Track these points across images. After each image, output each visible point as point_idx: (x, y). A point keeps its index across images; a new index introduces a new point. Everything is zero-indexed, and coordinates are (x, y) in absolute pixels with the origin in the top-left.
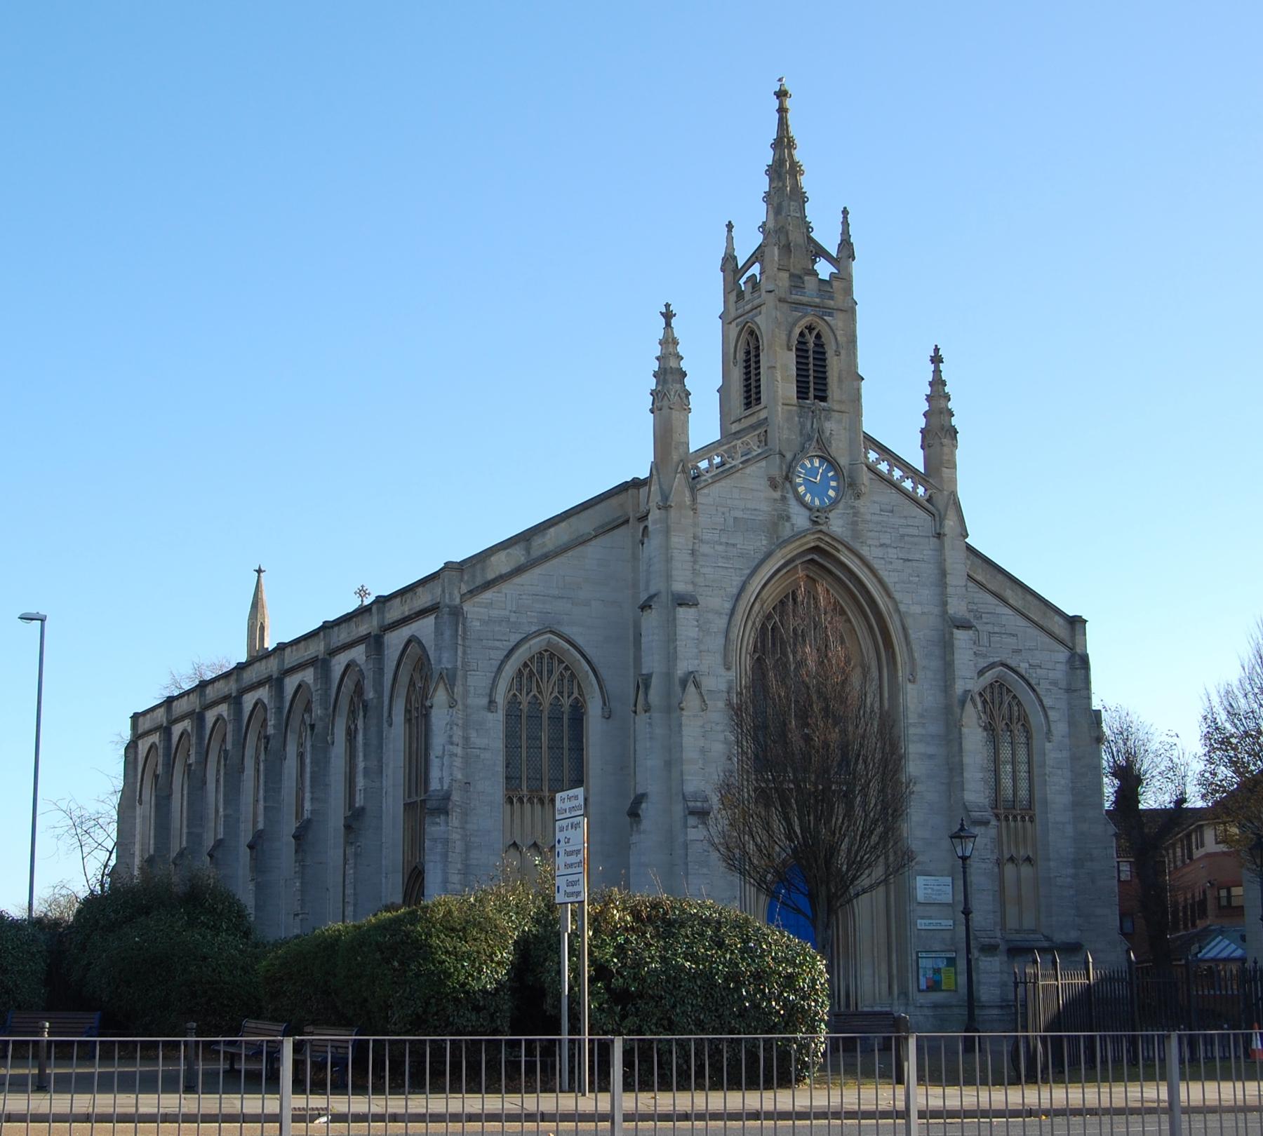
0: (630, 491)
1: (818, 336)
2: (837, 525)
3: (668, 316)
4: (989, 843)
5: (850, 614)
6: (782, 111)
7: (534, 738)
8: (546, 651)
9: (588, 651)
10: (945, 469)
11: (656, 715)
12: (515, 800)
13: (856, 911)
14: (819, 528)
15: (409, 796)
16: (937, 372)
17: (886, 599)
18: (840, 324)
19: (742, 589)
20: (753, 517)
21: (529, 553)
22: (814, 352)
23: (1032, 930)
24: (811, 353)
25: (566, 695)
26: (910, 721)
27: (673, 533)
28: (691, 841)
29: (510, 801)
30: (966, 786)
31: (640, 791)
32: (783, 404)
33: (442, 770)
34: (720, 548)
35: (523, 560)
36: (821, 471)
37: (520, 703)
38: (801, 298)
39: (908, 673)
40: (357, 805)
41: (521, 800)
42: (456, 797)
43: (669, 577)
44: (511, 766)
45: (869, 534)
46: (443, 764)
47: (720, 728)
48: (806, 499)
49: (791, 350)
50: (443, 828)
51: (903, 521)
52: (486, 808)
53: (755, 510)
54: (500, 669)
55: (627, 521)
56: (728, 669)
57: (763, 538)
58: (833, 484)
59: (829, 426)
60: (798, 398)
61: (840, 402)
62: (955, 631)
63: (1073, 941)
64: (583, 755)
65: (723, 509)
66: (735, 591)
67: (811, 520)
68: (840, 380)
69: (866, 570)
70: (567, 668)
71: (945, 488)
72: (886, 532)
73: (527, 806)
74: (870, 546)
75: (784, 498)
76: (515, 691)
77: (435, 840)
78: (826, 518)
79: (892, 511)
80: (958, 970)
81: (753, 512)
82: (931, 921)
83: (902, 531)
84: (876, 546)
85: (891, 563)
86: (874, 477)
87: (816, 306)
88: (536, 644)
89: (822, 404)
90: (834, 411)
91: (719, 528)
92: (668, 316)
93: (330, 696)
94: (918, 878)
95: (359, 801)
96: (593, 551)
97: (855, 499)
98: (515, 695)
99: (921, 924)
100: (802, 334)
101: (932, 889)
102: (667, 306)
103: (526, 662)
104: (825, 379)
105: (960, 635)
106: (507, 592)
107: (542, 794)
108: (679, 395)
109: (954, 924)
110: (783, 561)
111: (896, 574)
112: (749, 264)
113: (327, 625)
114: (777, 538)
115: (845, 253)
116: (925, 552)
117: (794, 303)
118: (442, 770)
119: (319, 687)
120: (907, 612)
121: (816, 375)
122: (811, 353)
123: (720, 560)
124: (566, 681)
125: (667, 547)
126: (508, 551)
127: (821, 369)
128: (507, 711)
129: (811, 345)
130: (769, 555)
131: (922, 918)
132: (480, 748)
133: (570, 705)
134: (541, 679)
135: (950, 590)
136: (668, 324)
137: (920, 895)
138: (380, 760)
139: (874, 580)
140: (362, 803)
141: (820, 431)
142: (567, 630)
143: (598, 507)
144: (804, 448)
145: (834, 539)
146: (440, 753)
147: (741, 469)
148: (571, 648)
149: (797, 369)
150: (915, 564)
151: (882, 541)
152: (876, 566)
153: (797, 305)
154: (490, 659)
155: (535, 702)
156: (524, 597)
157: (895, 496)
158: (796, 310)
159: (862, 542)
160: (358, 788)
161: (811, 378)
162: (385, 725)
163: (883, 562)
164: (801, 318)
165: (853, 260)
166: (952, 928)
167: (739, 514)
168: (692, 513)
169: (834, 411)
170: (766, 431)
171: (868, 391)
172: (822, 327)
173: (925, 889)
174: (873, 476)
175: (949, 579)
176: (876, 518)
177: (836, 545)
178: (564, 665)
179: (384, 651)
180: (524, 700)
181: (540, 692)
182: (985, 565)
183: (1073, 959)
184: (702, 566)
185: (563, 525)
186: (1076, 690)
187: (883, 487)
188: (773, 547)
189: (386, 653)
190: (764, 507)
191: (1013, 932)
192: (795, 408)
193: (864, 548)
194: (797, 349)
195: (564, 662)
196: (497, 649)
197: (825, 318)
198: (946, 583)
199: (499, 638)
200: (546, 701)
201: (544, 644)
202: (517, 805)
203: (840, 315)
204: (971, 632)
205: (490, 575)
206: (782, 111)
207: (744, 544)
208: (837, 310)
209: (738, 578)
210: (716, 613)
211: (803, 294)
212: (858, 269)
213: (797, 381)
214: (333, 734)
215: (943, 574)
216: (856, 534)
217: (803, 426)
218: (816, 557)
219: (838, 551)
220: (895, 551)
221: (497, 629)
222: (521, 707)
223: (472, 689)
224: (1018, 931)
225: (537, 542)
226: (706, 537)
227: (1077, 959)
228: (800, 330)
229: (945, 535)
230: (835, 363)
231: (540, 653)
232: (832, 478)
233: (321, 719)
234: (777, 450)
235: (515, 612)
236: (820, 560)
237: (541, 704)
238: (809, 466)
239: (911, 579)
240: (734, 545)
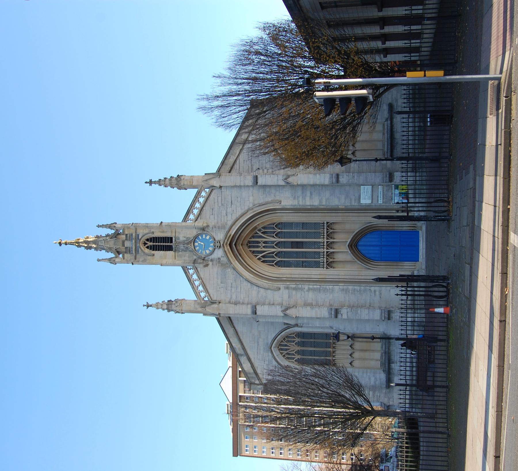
1: (147, 240)
2: (220, 236)
3: (148, 306)
4: (346, 174)
5: (256, 225)
6: (66, 244)
8: (278, 347)
9: (277, 332)
10: (194, 184)
13: (375, 223)
14: (222, 246)
16: (155, 183)
17: (248, 213)
18: (141, 231)
19: (249, 281)
20: (220, 275)
22: (154, 242)
23: (383, 126)
24: (154, 244)
25: (294, 340)
26: (297, 204)
28: (347, 317)
30: (322, 183)
32: (175, 259)
35: (245, 358)
36: (199, 242)
38: (133, 249)
45: (222, 221)
47: (303, 293)
48: (211, 249)
49: (154, 255)
51: (216, 203)
53: (217, 273)
57: (228, 270)
58: (204, 236)
59: (182, 239)
60: (172, 250)
61: (172, 232)
62: (258, 184)
63: (388, 107)
65: (218, 288)
66: (249, 284)
67: (219, 248)
68: (163, 232)
69: (237, 223)
71: (201, 184)
72: (221, 213)
74: (227, 221)
75: (212, 260)
78: (217, 242)
79: (213, 209)
81: (218, 275)
82: (379, 197)
83: (220, 205)
84: (227, 218)
85: (233, 210)
86: (200, 218)
87: (136, 243)
88: (276, 352)
89: (173, 240)
90: (175, 235)
91: (225, 290)
92: (148, 306)
94: (361, 203)
96: (239, 328)
97: (209, 227)
98: (295, 361)
99: (380, 201)
100: (147, 247)
101: (366, 195)
102: (144, 306)
103: (283, 356)
104: (163, 238)
105: (260, 182)
106: (257, 364)
108: (176, 307)
110: (236, 262)
111: (237, 208)
114: (227, 264)
115: (115, 228)
116: (228, 194)
117: (136, 253)
120: (253, 204)
121: (162, 242)
122: (154, 244)
124: (289, 339)
126: (242, 363)
127: (160, 249)
128: (302, 347)
129: (151, 244)
130: (234, 269)
133: (298, 338)
134: (289, 349)
135: (242, 184)
136: (151, 306)
137: (369, 202)
139: (241, 219)
141: (184, 243)
142: (270, 341)
144: (191, 251)
145: (226, 238)
147: (202, 280)
148: (276, 339)
149: (161, 250)
150: (233, 199)
151: (225, 215)
152: (235, 218)
153: (137, 251)
155: (298, 352)
157: (206, 208)
158: (138, 251)
159: (226, 224)
161: (164, 244)
163: (233, 214)
164: (141, 249)
165: (116, 223)
166: (382, 186)
167: (219, 281)
168: (220, 304)
169: (175, 235)
171: (167, 220)
172: (143, 239)
173: (366, 199)
174: (199, 218)
175: (238, 184)
176: (216, 218)
177: (228, 237)
180: (297, 357)
181: (294, 350)
182: (233, 148)
183: (395, 107)
184: (241, 299)
185: (231, 340)
187: (203, 213)
188: (231, 266)
191: (384, 136)
192: (176, 253)
193: (228, 224)
194: (154, 250)
195: (282, 341)
197: (140, 238)
198: (240, 186)
203: (138, 231)
204: (259, 176)
205: (252, 371)
206: (66, 244)
207: (231, 280)
208: (136, 233)
209: (244, 282)
210: (258, 293)
211: (132, 248)
213: (166, 250)
215: (236, 186)
216: (223, 227)
217: (183, 250)
218: (234, 243)
219: (230, 235)
220: (228, 208)
224: (384, 134)
226: (229, 296)
227: (395, 106)
228: (146, 249)
229: (220, 185)
230: (156, 234)
231: (279, 350)
232: (202, 237)
235: (265, 362)
236: (235, 241)
237: (298, 350)
239: (239, 201)
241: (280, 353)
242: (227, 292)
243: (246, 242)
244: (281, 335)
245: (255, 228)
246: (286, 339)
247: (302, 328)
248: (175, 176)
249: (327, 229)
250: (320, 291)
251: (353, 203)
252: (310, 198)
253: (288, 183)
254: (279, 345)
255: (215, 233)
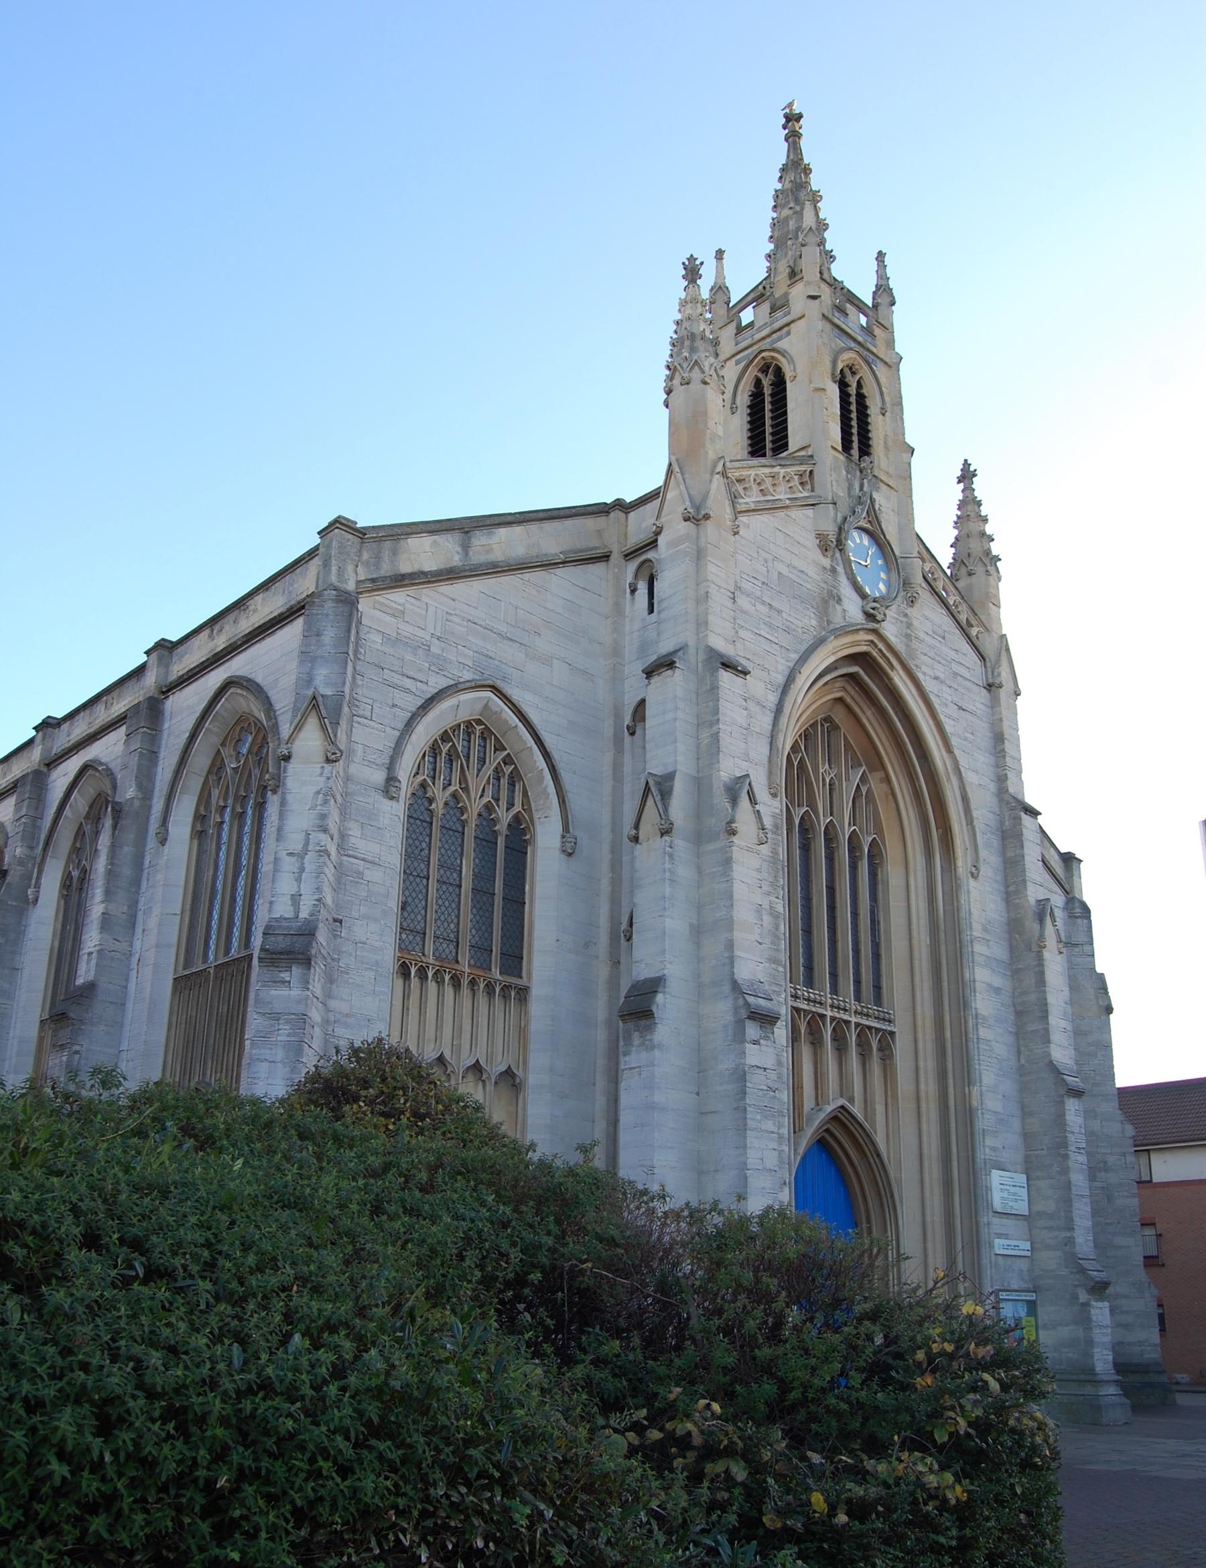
0: (612, 515)
7: (451, 867)
8: (479, 722)
11: (680, 844)
12: (413, 971)
15: (188, 963)
17: (944, 753)
21: (466, 554)
27: (709, 558)
29: (404, 971)
31: (643, 972)
33: (299, 880)
34: (763, 609)
35: (456, 560)
37: (431, 801)
39: (969, 865)
40: (80, 981)
41: (422, 973)
42: (322, 936)
43: (702, 624)
44: (409, 909)
45: (923, 657)
46: (302, 870)
50: (295, 992)
52: (367, 973)
54: (410, 725)
55: (605, 557)
56: (774, 795)
57: (812, 615)
64: (523, 913)
66: (781, 679)
70: (508, 760)
73: (432, 986)
76: (425, 777)
77: (275, 1017)
80: (1040, 1323)
85: (946, 705)
88: (465, 706)
93: (40, 828)
94: (994, 1171)
95: (85, 973)
96: (561, 581)
99: (1000, 1246)
107: (456, 967)
109: (1032, 1249)
110: (832, 659)
112: (743, 304)
113: (51, 721)
118: (299, 880)
119: (24, 812)
123: (762, 626)
125: (699, 578)
130: (819, 642)
131: (1000, 1236)
132: (363, 860)
138: (134, 905)
140: (91, 977)
142: (515, 694)
143: (569, 523)
146: (298, 847)
150: (968, 716)
154: (394, 706)
155: (456, 804)
156: (454, 619)
160: (86, 950)
162: (152, 842)
166: (1029, 1254)
167: (785, 571)
170: (811, 472)
172: (864, 372)
178: (505, 753)
179: (162, 724)
180: (440, 796)
181: (466, 789)
185: (518, 530)
186: (1076, 945)
189: (166, 725)
190: (812, 572)
196: (408, 691)
198: (1003, 750)
199: (411, 673)
200: (475, 807)
201: (479, 707)
202: (415, 981)
205: (405, 568)
212: (901, 318)
214: (38, 886)
219: (892, 667)
220: (948, 690)
221: (409, 657)
222: (434, 806)
223: (359, 749)
225: (480, 540)
233: (21, 862)
234: (830, 498)
238: (858, 541)
240: (779, 612)
241: (459, 725)
242: (755, 581)
243: (839, 716)
244: (535, 748)
245: (876, 763)
246: (508, 770)
247: (556, 854)
248: (995, 549)
249: (877, 1030)
250: (774, 962)
251: (989, 1142)
252: (988, 984)
253: (733, 795)
254: (487, 728)
255: (897, 619)
